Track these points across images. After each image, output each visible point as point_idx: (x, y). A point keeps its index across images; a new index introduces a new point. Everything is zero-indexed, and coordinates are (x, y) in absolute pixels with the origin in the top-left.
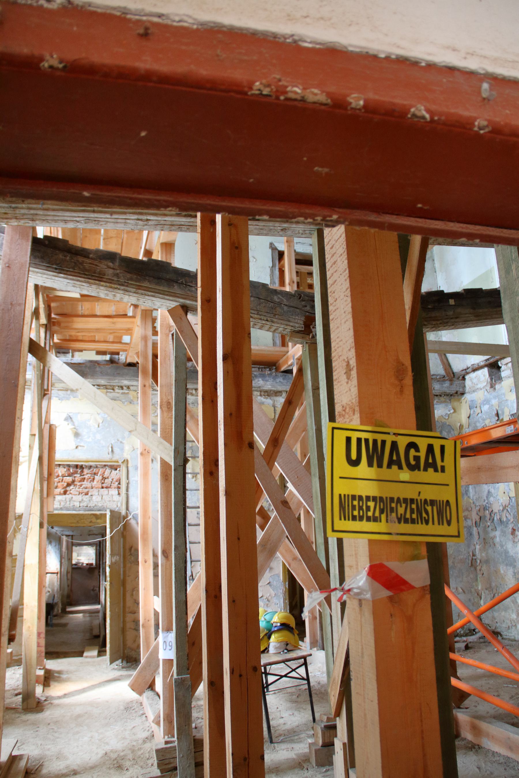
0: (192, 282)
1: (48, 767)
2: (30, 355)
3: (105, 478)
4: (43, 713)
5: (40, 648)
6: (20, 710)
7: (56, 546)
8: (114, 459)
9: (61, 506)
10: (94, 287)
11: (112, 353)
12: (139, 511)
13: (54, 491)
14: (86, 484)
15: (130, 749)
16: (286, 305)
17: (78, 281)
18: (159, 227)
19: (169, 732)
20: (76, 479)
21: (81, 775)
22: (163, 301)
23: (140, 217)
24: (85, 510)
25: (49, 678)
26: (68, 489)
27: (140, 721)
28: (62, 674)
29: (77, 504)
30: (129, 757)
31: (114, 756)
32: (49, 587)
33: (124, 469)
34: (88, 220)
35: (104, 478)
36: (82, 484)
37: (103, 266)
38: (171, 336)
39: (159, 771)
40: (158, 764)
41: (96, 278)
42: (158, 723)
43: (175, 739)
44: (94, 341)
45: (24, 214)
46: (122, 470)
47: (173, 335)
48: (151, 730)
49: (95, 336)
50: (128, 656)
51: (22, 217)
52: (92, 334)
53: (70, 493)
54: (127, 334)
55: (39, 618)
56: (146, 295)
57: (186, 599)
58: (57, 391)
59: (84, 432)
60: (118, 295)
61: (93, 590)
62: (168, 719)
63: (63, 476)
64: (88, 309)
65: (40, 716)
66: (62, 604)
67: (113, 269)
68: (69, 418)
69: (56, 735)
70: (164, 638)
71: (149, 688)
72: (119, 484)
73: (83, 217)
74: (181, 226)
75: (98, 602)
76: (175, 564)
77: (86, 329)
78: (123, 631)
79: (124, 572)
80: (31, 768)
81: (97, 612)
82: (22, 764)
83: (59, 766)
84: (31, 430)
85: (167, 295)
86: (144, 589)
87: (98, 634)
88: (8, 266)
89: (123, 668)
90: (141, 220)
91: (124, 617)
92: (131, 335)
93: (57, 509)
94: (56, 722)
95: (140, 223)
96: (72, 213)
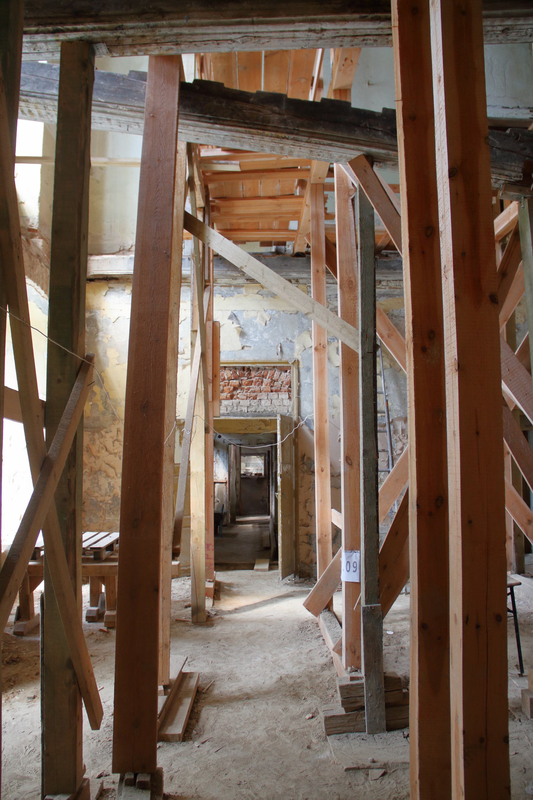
0: (377, 125)
1: (220, 687)
2: (185, 231)
3: (275, 381)
4: (214, 627)
5: (209, 561)
6: (190, 623)
7: (223, 455)
8: (284, 360)
9: (228, 412)
10: (257, 138)
11: (278, 244)
12: (314, 414)
13: (220, 395)
14: (253, 387)
15: (307, 676)
16: (499, 149)
17: (237, 131)
18: (337, 41)
19: (353, 663)
20: (243, 382)
21: (255, 700)
22: (342, 150)
23: (313, 26)
24: (253, 416)
25: (218, 592)
26: (235, 393)
27: (317, 644)
28: (233, 587)
29: (245, 409)
30: (306, 685)
31: (290, 682)
32: (218, 497)
33: (294, 370)
34: (246, 37)
35: (273, 381)
36: (250, 388)
37: (266, 111)
38: (350, 201)
39: (343, 709)
40: (342, 701)
41: (259, 127)
42: (339, 652)
43: (362, 674)
44: (258, 230)
45: (165, 36)
46: (293, 371)
47: (353, 200)
48: (329, 656)
49: (258, 223)
50: (302, 572)
51: (163, 41)
52: (256, 221)
53: (238, 398)
54: (294, 219)
55: (207, 529)
56: (320, 144)
57: (378, 514)
58: (219, 287)
59: (250, 331)
60: (287, 147)
61: (262, 500)
62: (353, 650)
63: (229, 379)
64: (250, 189)
65: (210, 631)
66: (232, 514)
67: (279, 114)
68: (233, 317)
69: (227, 652)
70: (347, 558)
71: (326, 608)
72: (290, 387)
73: (239, 33)
74: (366, 38)
75: (268, 513)
76: (364, 472)
77: (248, 215)
78: (296, 544)
79: (297, 482)
80: (203, 686)
81: (267, 523)
82: (193, 683)
83: (231, 687)
84: (192, 326)
85: (347, 143)
86: (321, 501)
87: (269, 546)
88: (153, 116)
89: (295, 583)
90: (314, 31)
91: (297, 530)
92: (299, 219)
93: (223, 415)
94: (227, 639)
95: (313, 35)
96: (226, 28)
